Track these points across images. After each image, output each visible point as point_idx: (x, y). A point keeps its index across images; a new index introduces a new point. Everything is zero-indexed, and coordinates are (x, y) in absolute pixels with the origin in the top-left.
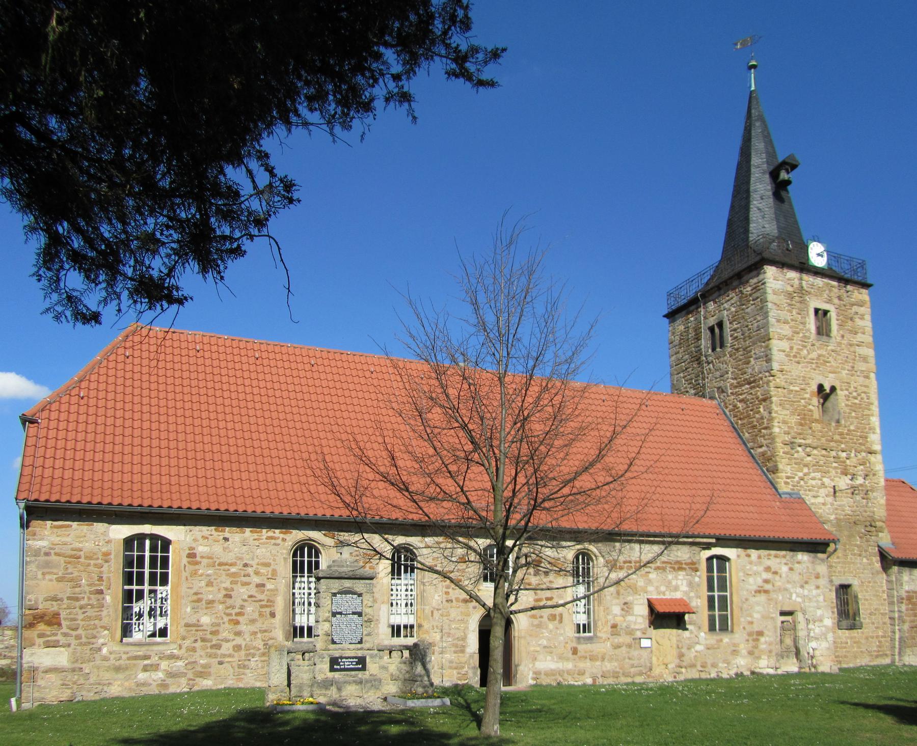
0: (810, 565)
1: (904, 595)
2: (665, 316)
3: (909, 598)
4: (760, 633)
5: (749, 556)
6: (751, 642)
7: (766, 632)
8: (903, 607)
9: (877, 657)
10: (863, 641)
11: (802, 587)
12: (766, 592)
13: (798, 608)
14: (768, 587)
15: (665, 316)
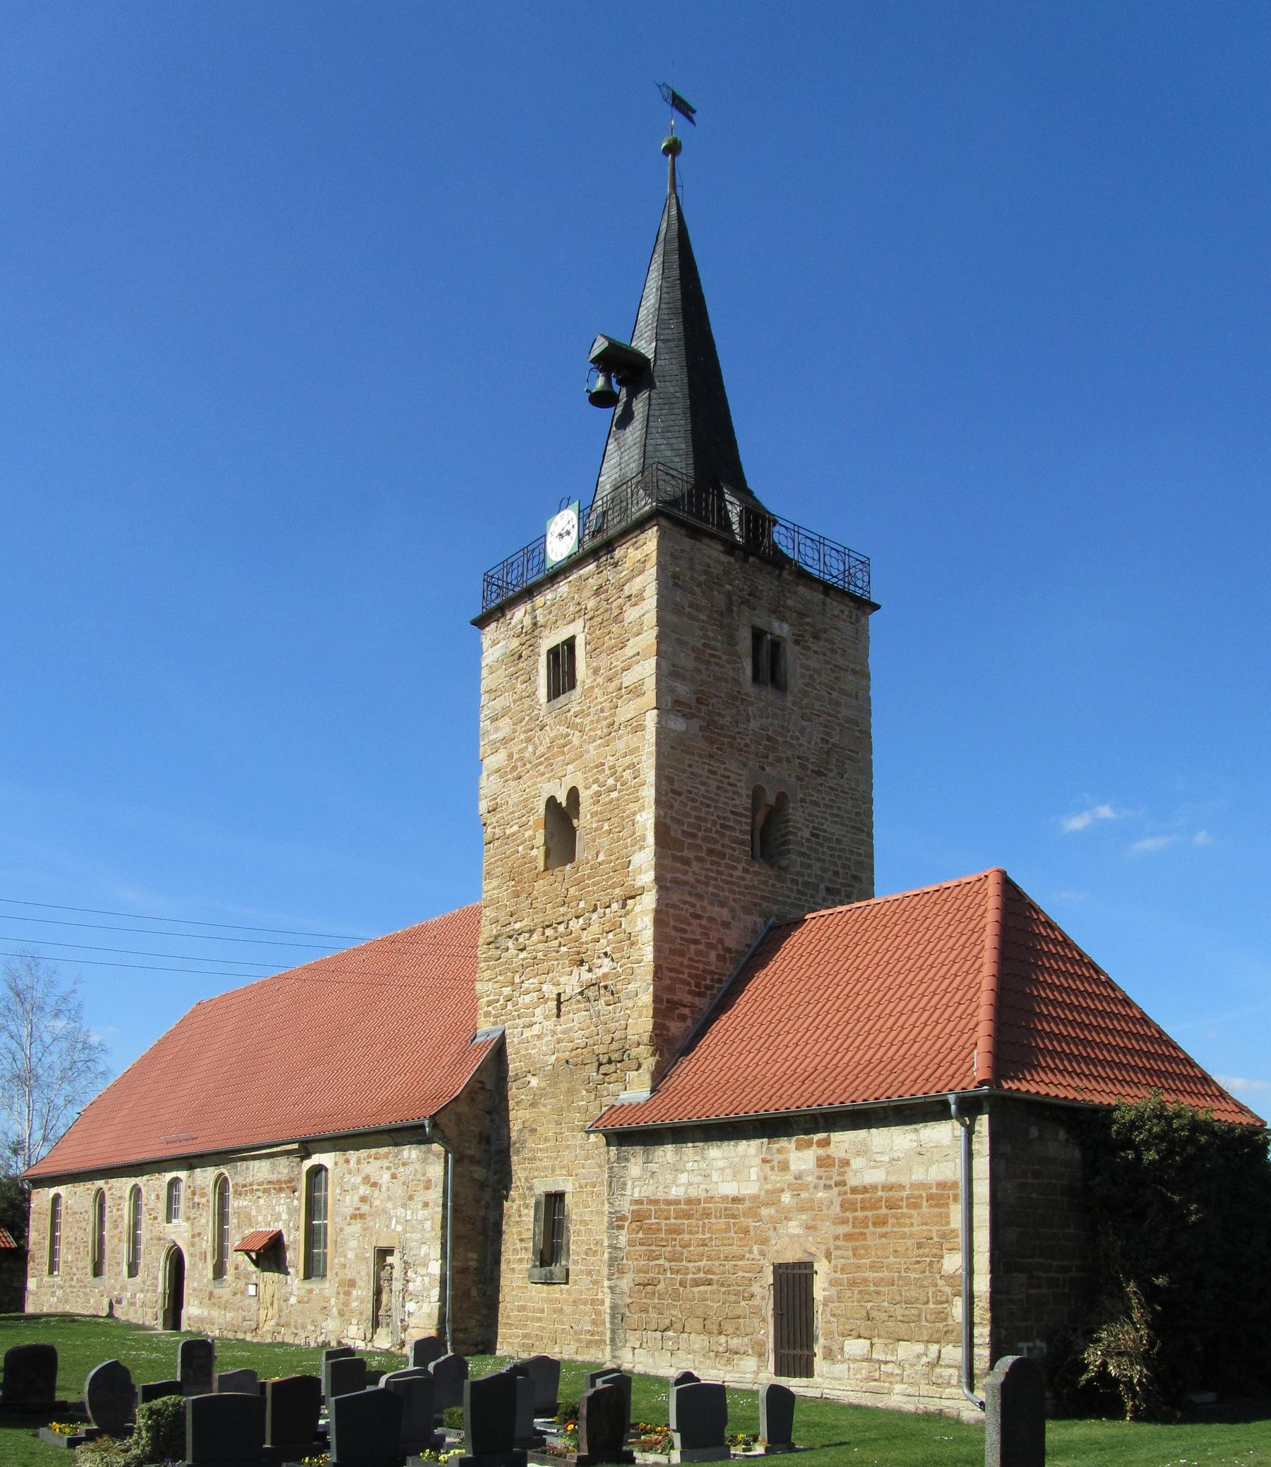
0: (418, 1166)
1: (626, 1207)
2: (876, 607)
3: (639, 1217)
4: (352, 1283)
5: (347, 1161)
6: (342, 1296)
7: (359, 1283)
8: (623, 1238)
9: (589, 1344)
10: (568, 1309)
11: (404, 1206)
12: (362, 1216)
13: (395, 1243)
14: (365, 1208)
15: (876, 607)
